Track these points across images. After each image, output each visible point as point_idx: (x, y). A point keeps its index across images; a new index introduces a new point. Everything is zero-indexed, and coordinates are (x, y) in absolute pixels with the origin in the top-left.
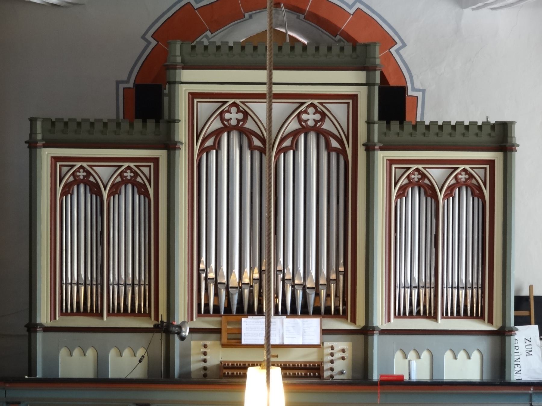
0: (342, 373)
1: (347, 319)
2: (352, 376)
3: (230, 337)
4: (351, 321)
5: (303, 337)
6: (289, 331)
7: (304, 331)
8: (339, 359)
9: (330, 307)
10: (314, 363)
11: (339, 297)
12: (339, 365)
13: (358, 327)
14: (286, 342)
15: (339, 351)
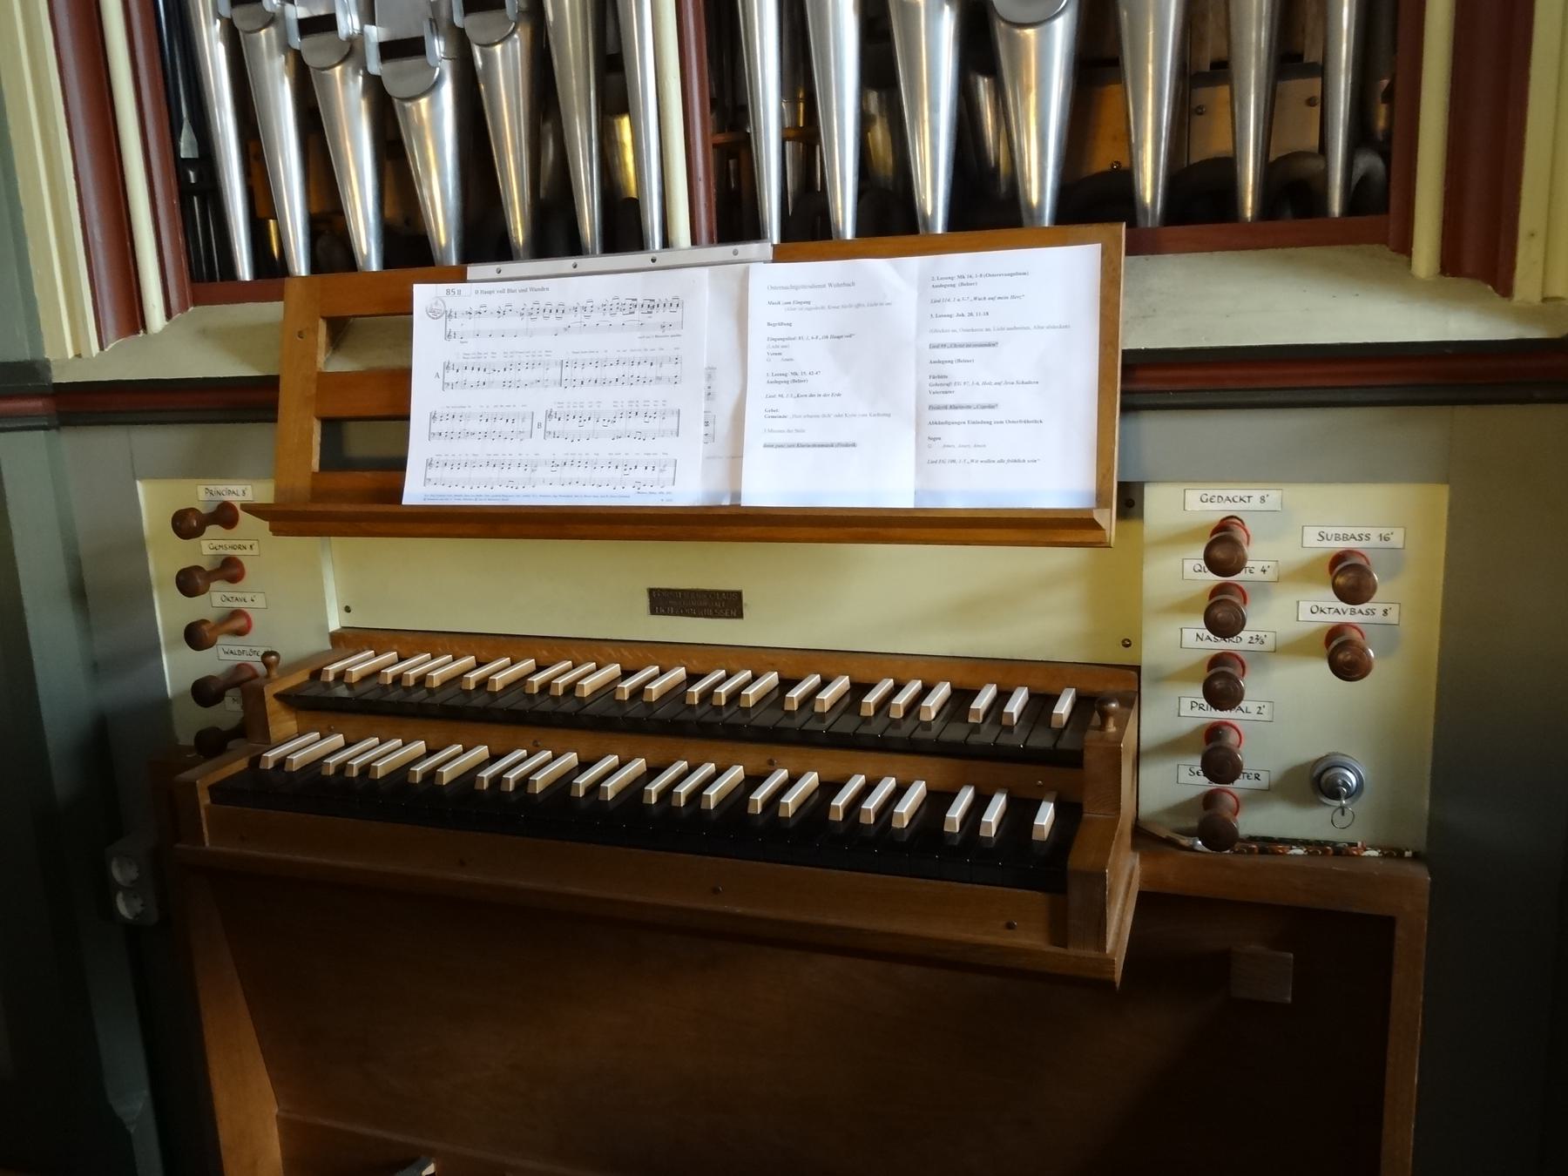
0: (1317, 783)
1: (1404, 246)
2: (1436, 828)
3: (769, 441)
4: (1451, 264)
5: (925, 439)
6: (796, 378)
7: (941, 382)
8: (1295, 649)
9: (1227, 167)
10: (1042, 679)
11: (1321, 70)
12: (1291, 711)
13: (1525, 314)
14: (764, 488)
15: (1302, 575)
